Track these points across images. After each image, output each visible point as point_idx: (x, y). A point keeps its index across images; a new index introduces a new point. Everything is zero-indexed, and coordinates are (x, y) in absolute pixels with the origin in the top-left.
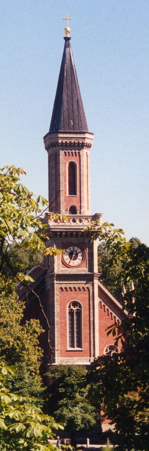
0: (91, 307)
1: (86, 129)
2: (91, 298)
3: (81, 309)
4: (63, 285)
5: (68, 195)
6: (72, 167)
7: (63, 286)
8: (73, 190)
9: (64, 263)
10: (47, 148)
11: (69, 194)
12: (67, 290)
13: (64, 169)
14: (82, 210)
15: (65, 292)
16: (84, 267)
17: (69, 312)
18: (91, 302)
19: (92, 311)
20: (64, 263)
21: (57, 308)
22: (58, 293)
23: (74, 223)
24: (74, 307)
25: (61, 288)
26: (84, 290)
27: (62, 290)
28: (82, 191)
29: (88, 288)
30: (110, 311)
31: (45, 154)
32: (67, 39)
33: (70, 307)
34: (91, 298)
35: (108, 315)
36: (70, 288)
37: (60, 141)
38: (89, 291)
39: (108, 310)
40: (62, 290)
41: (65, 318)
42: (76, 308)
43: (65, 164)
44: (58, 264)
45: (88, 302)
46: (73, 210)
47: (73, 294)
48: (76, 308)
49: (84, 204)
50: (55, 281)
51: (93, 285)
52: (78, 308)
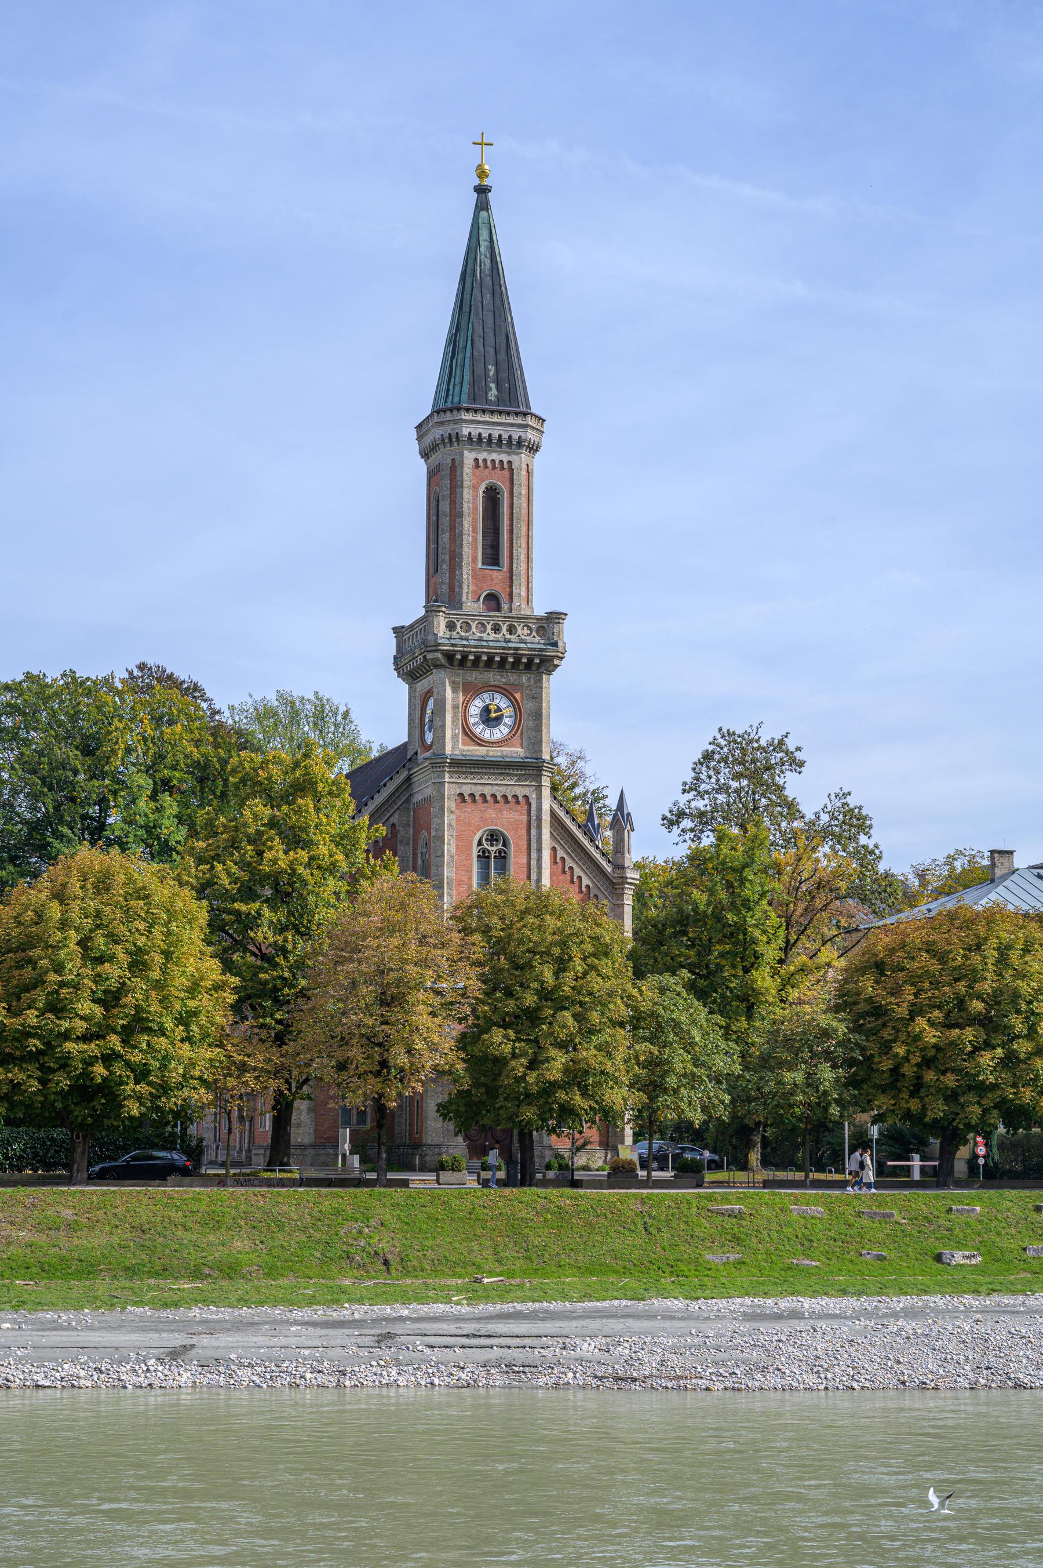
0: (534, 845)
1: (528, 406)
2: (534, 824)
3: (509, 850)
4: (464, 787)
5: (480, 565)
6: (492, 496)
7: (466, 790)
8: (492, 556)
9: (468, 732)
10: (425, 454)
11: (483, 564)
12: (474, 801)
13: (472, 501)
14: (516, 603)
15: (469, 807)
16: (513, 746)
17: (479, 856)
18: (533, 832)
19: (534, 855)
20: (468, 732)
21: (449, 844)
22: (453, 805)
23: (438, 1105)
24: (492, 845)
25: (461, 795)
26: (518, 803)
27: (464, 801)
28: (515, 531)
29: (526, 797)
30: (569, 863)
31: (420, 469)
32: (482, 191)
33: (480, 843)
34: (532, 823)
35: (564, 872)
36: (483, 796)
37: (465, 432)
38: (529, 804)
39: (563, 859)
40: (464, 801)
41: (470, 871)
42: (494, 848)
43: (475, 488)
44: (454, 736)
45: (524, 832)
46: (493, 601)
47: (491, 812)
48: (494, 848)
49: (520, 590)
50: (447, 775)
51: (539, 788)
52: (500, 847)
